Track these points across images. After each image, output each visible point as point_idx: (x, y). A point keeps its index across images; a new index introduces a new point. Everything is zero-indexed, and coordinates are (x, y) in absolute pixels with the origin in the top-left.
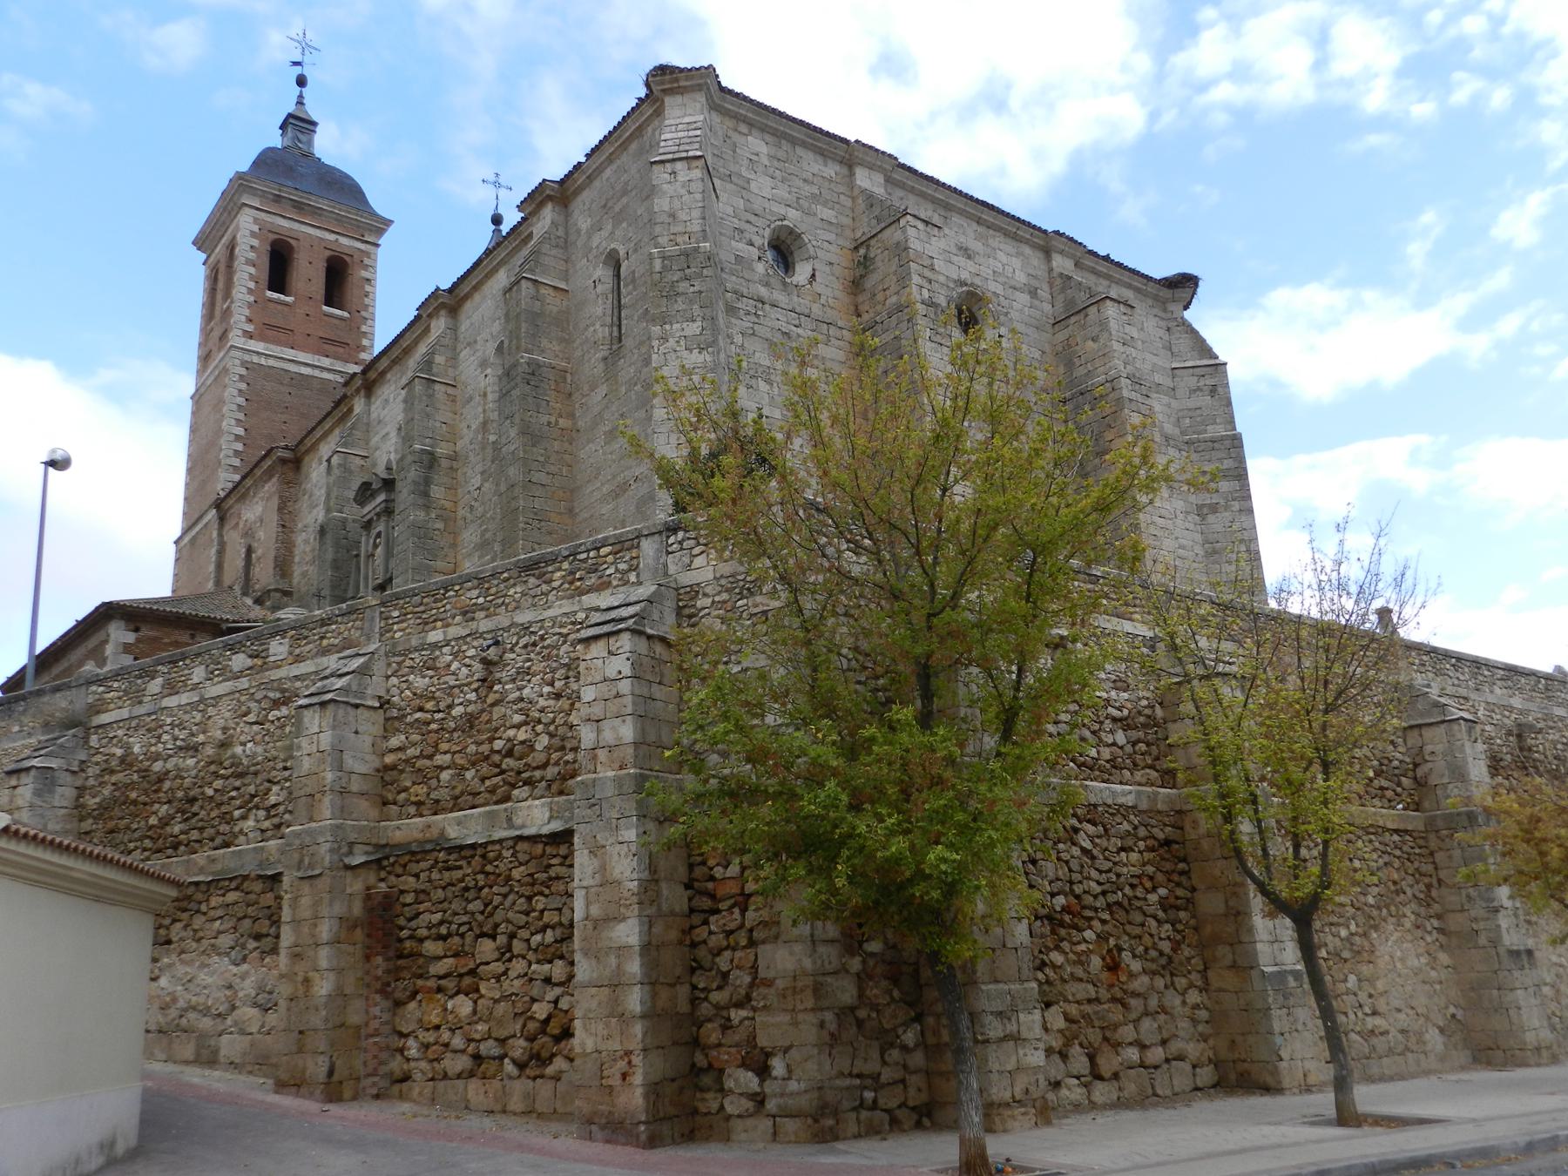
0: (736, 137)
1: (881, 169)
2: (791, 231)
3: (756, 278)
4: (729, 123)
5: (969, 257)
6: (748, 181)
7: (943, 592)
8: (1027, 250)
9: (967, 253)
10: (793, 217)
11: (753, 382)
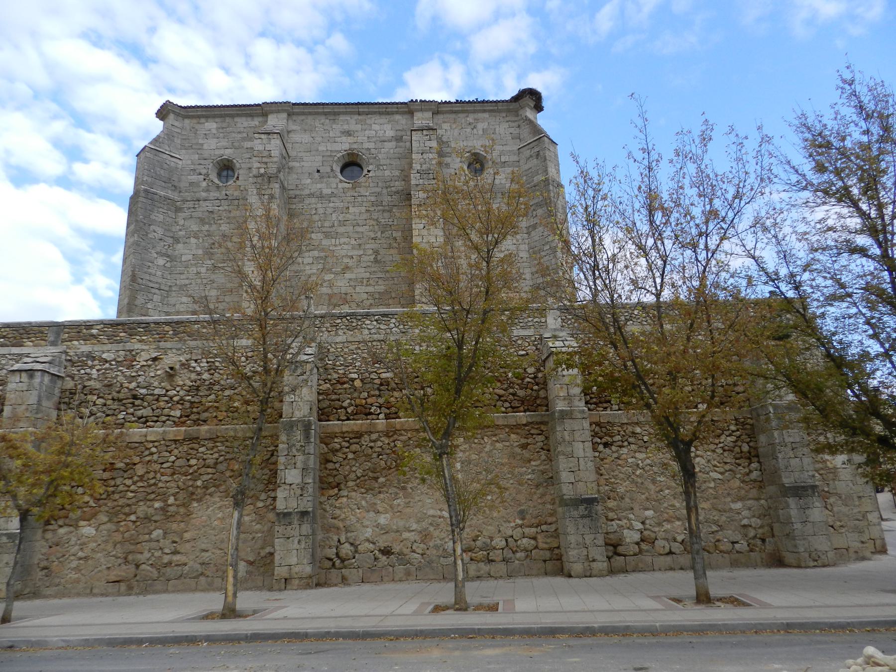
0: (197, 126)
1: (283, 111)
2: (228, 160)
3: (201, 189)
4: (195, 121)
5: (350, 135)
6: (202, 145)
7: (659, 288)
8: (397, 117)
9: (348, 133)
10: (228, 153)
11: (188, 241)
